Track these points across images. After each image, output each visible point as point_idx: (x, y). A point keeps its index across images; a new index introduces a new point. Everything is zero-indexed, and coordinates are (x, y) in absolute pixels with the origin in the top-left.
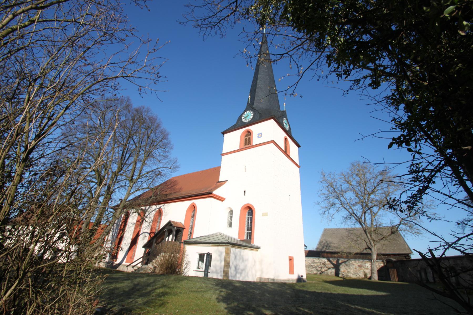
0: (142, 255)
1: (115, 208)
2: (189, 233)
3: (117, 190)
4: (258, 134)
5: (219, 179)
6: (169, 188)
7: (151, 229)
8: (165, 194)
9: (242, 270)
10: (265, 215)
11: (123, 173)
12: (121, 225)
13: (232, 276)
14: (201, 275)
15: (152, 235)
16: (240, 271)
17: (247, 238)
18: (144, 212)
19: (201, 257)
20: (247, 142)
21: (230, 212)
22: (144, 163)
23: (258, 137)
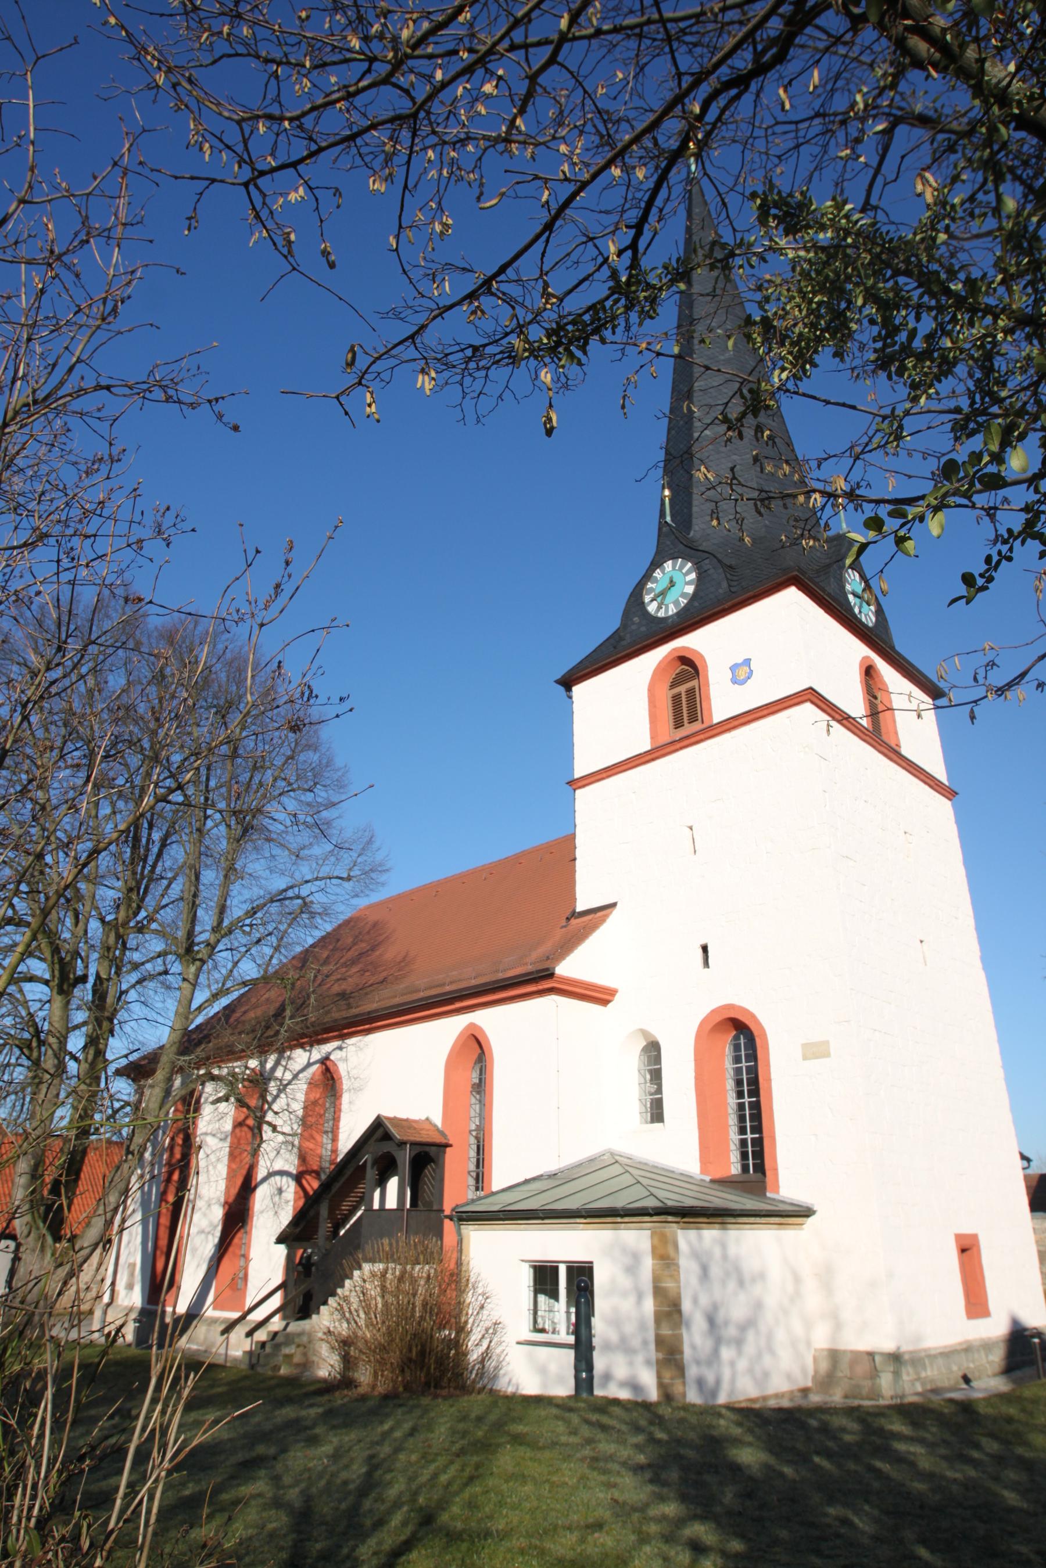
0: (278, 1279)
1: (139, 1070)
2: (472, 1167)
3: (132, 995)
4: (734, 668)
5: (573, 899)
6: (354, 962)
7: (303, 1158)
8: (342, 990)
9: (745, 1327)
10: (815, 1051)
11: (151, 919)
12: (171, 1148)
13: (698, 1363)
14: (564, 1389)
15: (313, 1184)
16: (731, 1331)
17: (745, 1168)
18: (260, 1081)
19: (544, 1277)
20: (684, 713)
21: (645, 1049)
22: (231, 873)
23: (735, 681)
